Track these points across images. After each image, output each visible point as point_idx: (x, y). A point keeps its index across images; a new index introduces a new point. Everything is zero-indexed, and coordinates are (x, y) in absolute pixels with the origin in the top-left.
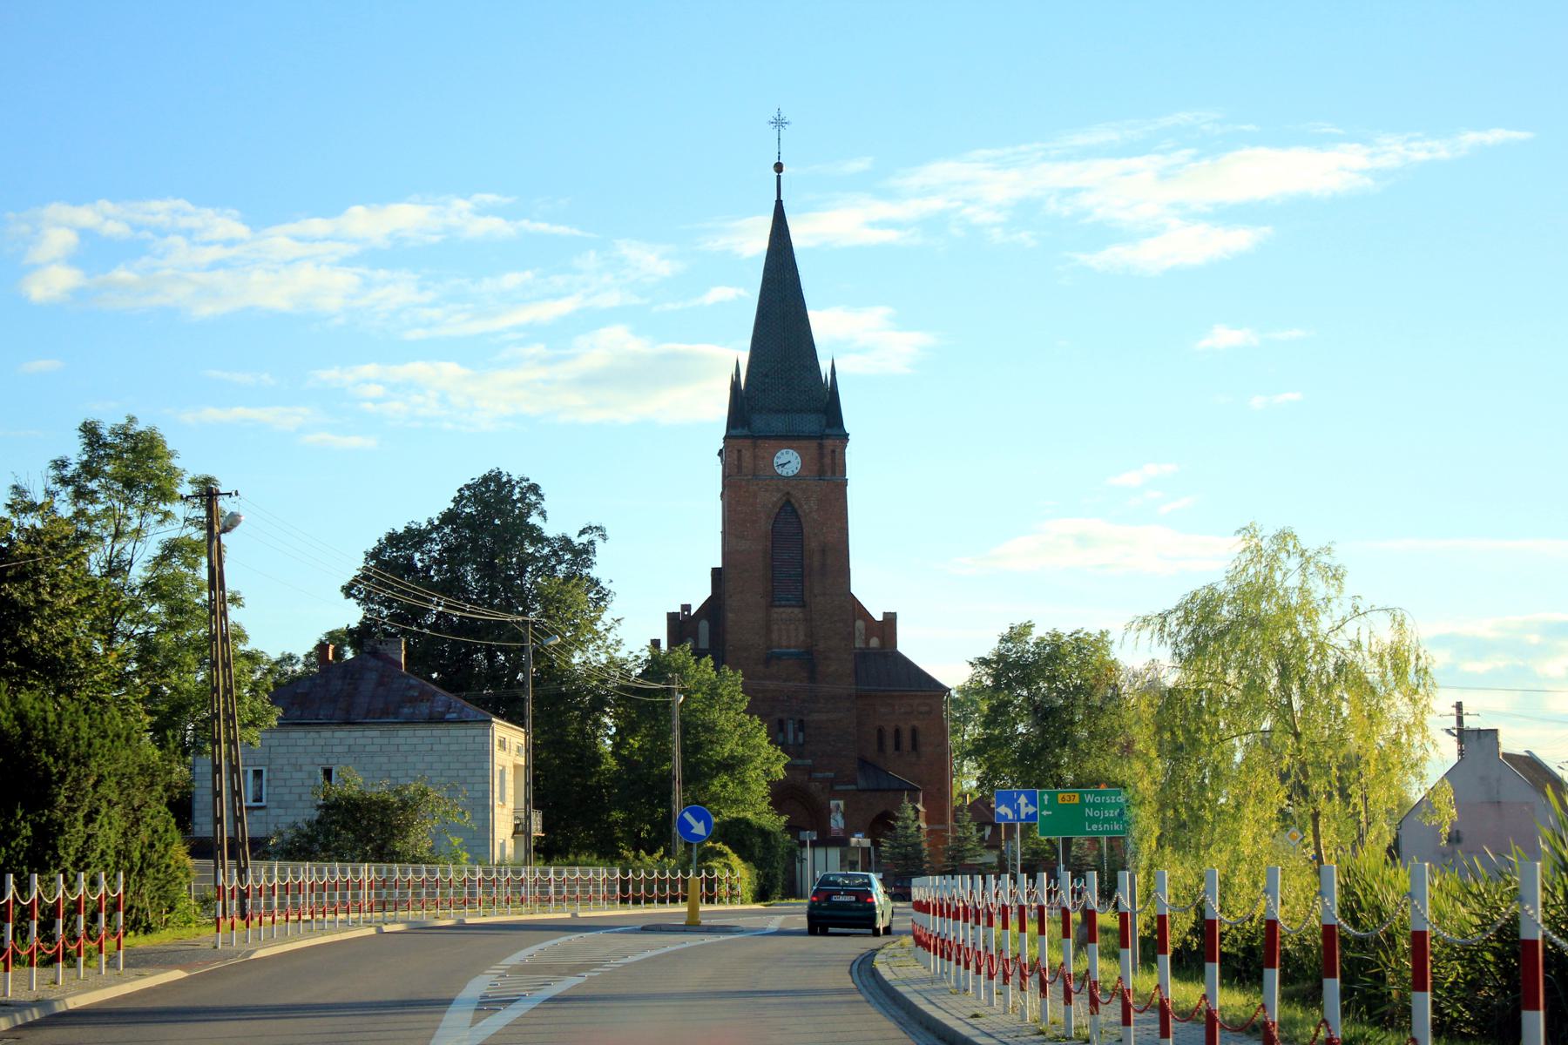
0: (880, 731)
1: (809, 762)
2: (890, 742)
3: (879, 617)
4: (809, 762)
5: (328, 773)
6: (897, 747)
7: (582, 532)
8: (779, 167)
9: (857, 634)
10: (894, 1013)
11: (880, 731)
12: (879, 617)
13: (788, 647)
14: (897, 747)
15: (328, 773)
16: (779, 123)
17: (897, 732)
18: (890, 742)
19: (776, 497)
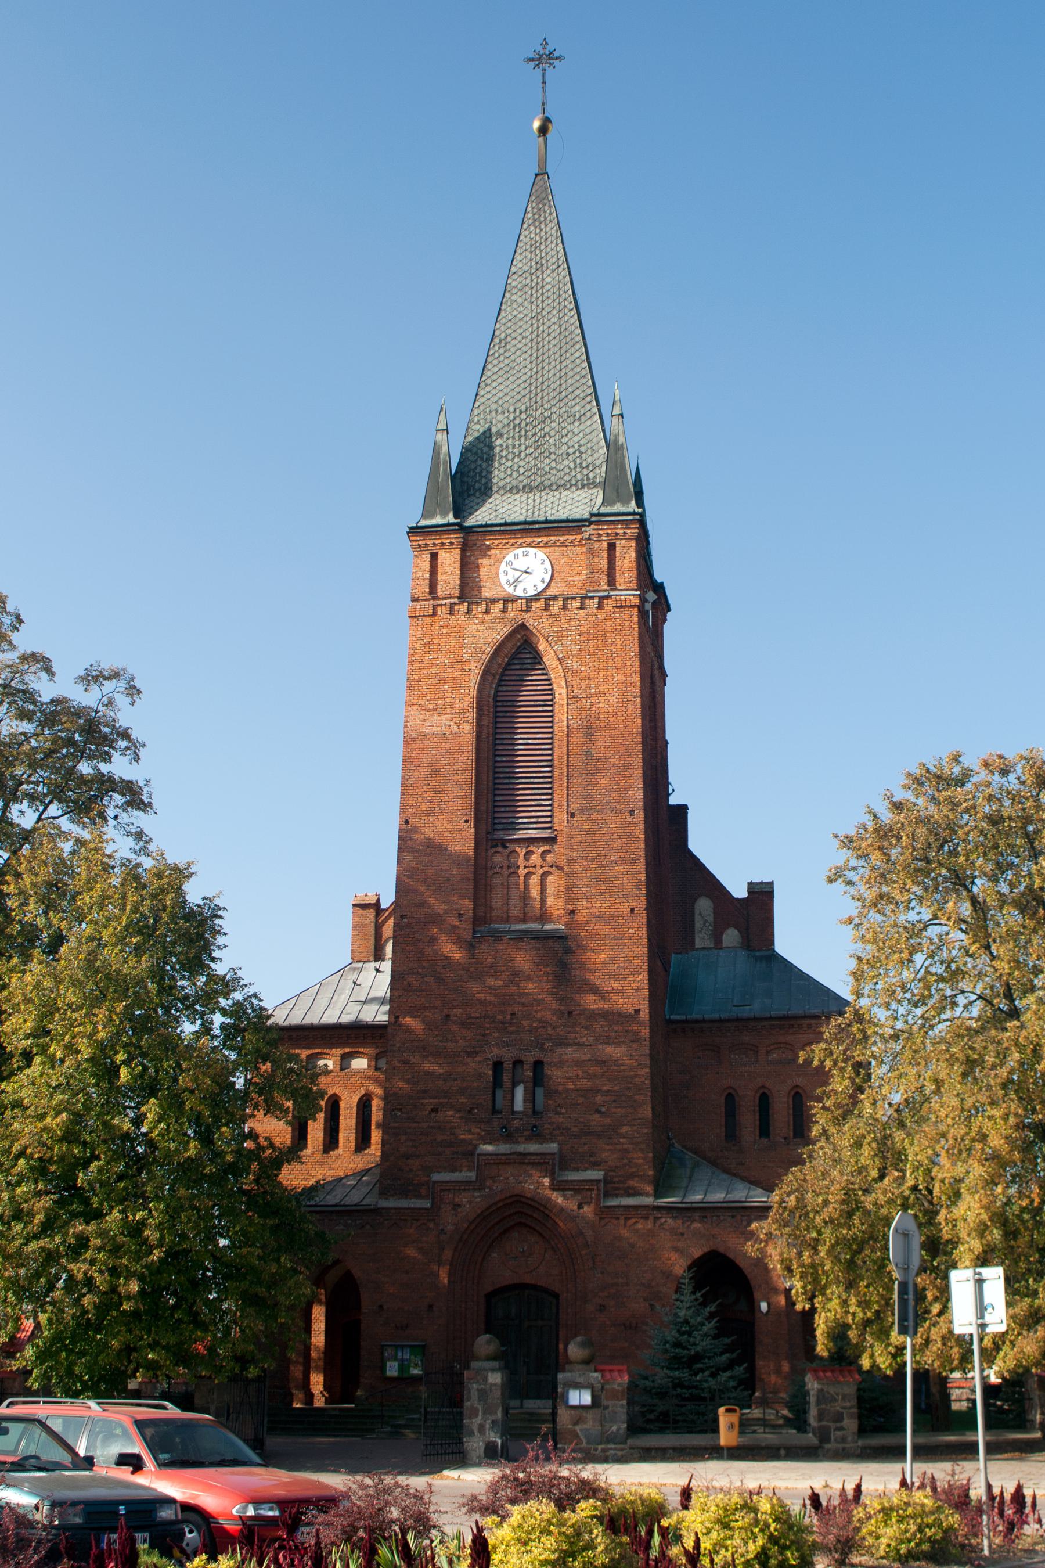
0: (731, 1100)
1: (553, 1147)
2: (748, 1120)
3: (740, 892)
4: (553, 1147)
5: (836, 837)
6: (765, 1129)
7: (92, 678)
8: (544, 82)
9: (698, 925)
10: (483, 808)
11: (731, 1100)
12: (740, 892)
13: (610, 1371)
14: (765, 1129)
15: (836, 837)
16: (545, 58)
17: (764, 1101)
18: (748, 1120)
19: (500, 631)
